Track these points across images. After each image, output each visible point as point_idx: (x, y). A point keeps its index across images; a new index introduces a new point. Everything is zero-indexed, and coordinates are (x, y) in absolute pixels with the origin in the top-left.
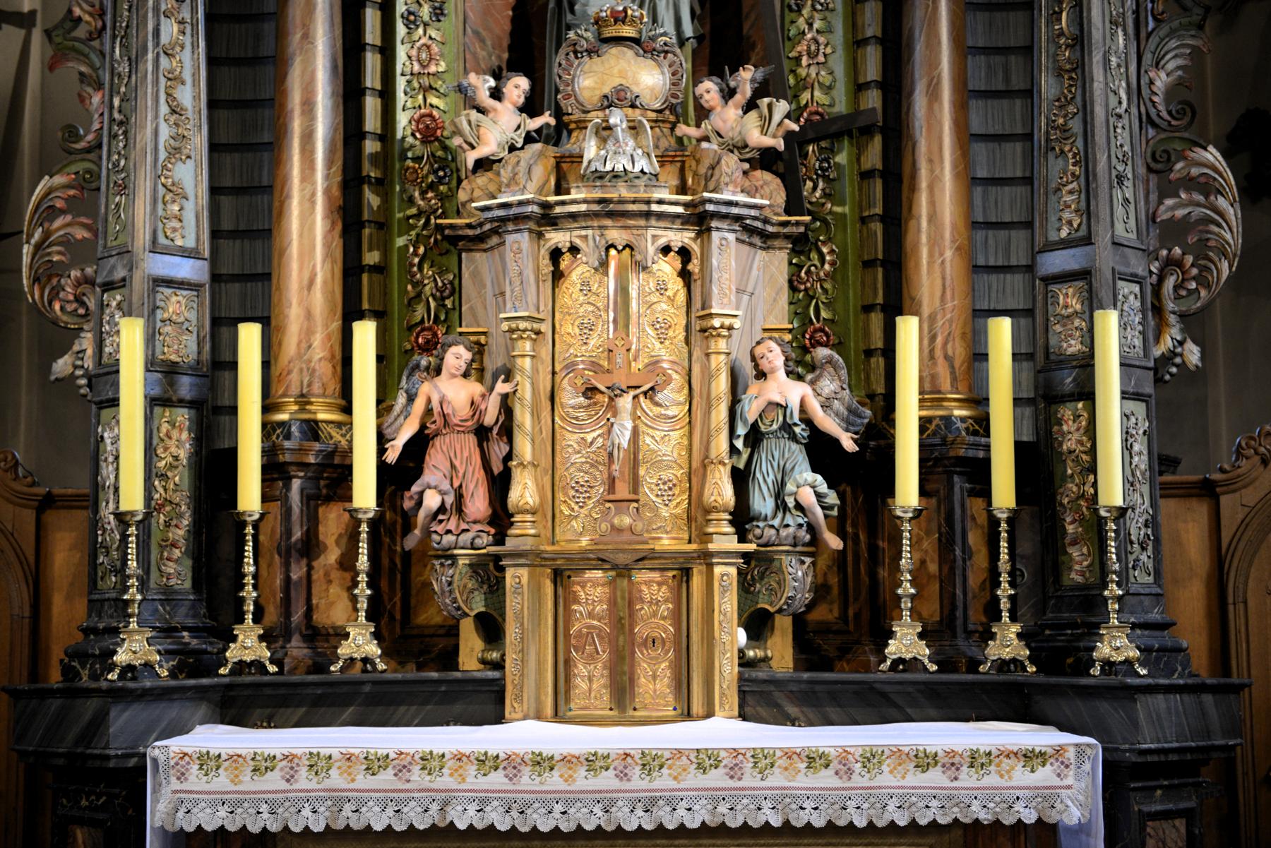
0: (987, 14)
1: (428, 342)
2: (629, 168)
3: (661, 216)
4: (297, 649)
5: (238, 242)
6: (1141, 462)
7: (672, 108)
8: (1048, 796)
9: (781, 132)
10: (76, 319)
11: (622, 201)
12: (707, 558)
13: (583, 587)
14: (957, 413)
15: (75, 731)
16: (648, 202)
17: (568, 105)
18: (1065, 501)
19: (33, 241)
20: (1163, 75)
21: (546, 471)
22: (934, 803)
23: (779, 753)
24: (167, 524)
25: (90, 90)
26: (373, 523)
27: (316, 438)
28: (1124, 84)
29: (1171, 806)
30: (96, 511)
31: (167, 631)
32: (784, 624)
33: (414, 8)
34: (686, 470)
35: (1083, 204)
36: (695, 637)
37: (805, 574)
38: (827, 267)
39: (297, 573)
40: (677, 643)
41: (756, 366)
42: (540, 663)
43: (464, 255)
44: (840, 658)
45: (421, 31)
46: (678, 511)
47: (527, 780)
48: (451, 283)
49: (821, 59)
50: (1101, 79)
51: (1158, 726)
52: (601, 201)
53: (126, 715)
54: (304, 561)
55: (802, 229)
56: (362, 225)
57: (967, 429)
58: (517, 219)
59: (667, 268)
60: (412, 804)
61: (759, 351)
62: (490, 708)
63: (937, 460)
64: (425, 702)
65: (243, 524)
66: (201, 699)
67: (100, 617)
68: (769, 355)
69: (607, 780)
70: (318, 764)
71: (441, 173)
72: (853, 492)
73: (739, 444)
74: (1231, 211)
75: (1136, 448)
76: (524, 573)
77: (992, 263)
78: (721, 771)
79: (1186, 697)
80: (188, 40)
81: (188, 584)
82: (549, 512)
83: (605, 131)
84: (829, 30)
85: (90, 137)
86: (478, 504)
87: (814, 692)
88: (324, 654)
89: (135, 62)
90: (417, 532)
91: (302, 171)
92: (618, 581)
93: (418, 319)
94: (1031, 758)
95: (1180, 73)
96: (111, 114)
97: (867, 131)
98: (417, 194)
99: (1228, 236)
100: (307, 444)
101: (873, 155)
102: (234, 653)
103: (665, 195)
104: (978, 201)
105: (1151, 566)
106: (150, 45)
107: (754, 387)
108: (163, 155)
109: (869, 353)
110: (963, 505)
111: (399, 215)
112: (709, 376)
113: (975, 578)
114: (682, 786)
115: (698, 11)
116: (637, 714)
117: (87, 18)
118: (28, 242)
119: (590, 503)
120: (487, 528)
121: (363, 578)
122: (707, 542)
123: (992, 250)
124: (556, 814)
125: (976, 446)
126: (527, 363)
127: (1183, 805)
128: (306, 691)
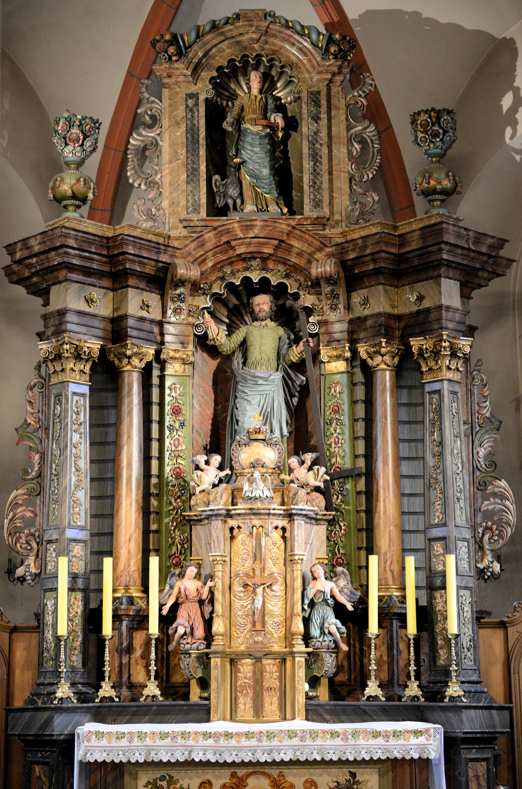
0: (408, 426)
1: (177, 562)
2: (261, 495)
3: (274, 515)
4: (125, 692)
5: (97, 519)
6: (468, 614)
7: (279, 467)
8: (422, 748)
9: (322, 480)
10: (26, 551)
11: (258, 509)
12: (292, 654)
13: (242, 666)
14: (395, 594)
15: (38, 725)
16: (269, 509)
17: (236, 466)
18: (438, 631)
19: (9, 518)
20: (483, 450)
21: (227, 618)
22: (380, 751)
23: (320, 731)
24: (73, 640)
25: (34, 453)
26: (156, 640)
27: (132, 604)
28: (460, 460)
29: (479, 756)
30: (43, 634)
31: (73, 684)
32: (325, 682)
33: (172, 423)
34: (284, 618)
35: (443, 511)
37: (333, 661)
38: (343, 531)
39: (125, 660)
40: (280, 689)
41: (313, 575)
42: (225, 697)
43: (193, 527)
44: (348, 696)
45: (175, 432)
46: (281, 635)
47: (222, 742)
48: (187, 537)
49: (340, 445)
50: (450, 459)
51: (471, 722)
52: (250, 509)
53: (60, 718)
54: (128, 655)
55: (332, 517)
56: (150, 513)
57: (399, 601)
58: (216, 515)
59: (276, 535)
60: (178, 751)
63: (386, 614)
64: (177, 715)
65: (105, 640)
66: (87, 712)
67: (45, 678)
68: (318, 571)
69: (253, 742)
70: (141, 736)
71: (183, 492)
72: (353, 626)
73: (306, 607)
74: (511, 507)
75: (466, 609)
76: (218, 660)
77: (411, 529)
78: (297, 738)
79: (484, 711)
80: (82, 441)
81: (81, 665)
82: (229, 635)
83: (251, 481)
85: (33, 474)
86: (200, 632)
87: (336, 710)
88: (135, 694)
89: (63, 450)
90: (174, 643)
91: (127, 493)
92: (257, 664)
93: (173, 553)
94: (417, 733)
95: (490, 449)
96: (51, 471)
97: (359, 475)
98: (173, 500)
100: (130, 607)
101: (362, 485)
102: (101, 693)
103: (275, 506)
104: (405, 504)
105: (472, 658)
106: (69, 444)
107: (312, 583)
108: (73, 488)
109: (360, 567)
110: (397, 632)
111: (166, 510)
112: (293, 579)
113: (402, 664)
114: (282, 744)
115: (289, 422)
116: (264, 719)
117: (33, 423)
118: (7, 518)
119: (246, 632)
120: (204, 642)
121: (153, 662)
122: (292, 648)
123: (411, 524)
124: (234, 756)
125: (401, 608)
126: (220, 574)
127: (485, 756)
128: (129, 709)
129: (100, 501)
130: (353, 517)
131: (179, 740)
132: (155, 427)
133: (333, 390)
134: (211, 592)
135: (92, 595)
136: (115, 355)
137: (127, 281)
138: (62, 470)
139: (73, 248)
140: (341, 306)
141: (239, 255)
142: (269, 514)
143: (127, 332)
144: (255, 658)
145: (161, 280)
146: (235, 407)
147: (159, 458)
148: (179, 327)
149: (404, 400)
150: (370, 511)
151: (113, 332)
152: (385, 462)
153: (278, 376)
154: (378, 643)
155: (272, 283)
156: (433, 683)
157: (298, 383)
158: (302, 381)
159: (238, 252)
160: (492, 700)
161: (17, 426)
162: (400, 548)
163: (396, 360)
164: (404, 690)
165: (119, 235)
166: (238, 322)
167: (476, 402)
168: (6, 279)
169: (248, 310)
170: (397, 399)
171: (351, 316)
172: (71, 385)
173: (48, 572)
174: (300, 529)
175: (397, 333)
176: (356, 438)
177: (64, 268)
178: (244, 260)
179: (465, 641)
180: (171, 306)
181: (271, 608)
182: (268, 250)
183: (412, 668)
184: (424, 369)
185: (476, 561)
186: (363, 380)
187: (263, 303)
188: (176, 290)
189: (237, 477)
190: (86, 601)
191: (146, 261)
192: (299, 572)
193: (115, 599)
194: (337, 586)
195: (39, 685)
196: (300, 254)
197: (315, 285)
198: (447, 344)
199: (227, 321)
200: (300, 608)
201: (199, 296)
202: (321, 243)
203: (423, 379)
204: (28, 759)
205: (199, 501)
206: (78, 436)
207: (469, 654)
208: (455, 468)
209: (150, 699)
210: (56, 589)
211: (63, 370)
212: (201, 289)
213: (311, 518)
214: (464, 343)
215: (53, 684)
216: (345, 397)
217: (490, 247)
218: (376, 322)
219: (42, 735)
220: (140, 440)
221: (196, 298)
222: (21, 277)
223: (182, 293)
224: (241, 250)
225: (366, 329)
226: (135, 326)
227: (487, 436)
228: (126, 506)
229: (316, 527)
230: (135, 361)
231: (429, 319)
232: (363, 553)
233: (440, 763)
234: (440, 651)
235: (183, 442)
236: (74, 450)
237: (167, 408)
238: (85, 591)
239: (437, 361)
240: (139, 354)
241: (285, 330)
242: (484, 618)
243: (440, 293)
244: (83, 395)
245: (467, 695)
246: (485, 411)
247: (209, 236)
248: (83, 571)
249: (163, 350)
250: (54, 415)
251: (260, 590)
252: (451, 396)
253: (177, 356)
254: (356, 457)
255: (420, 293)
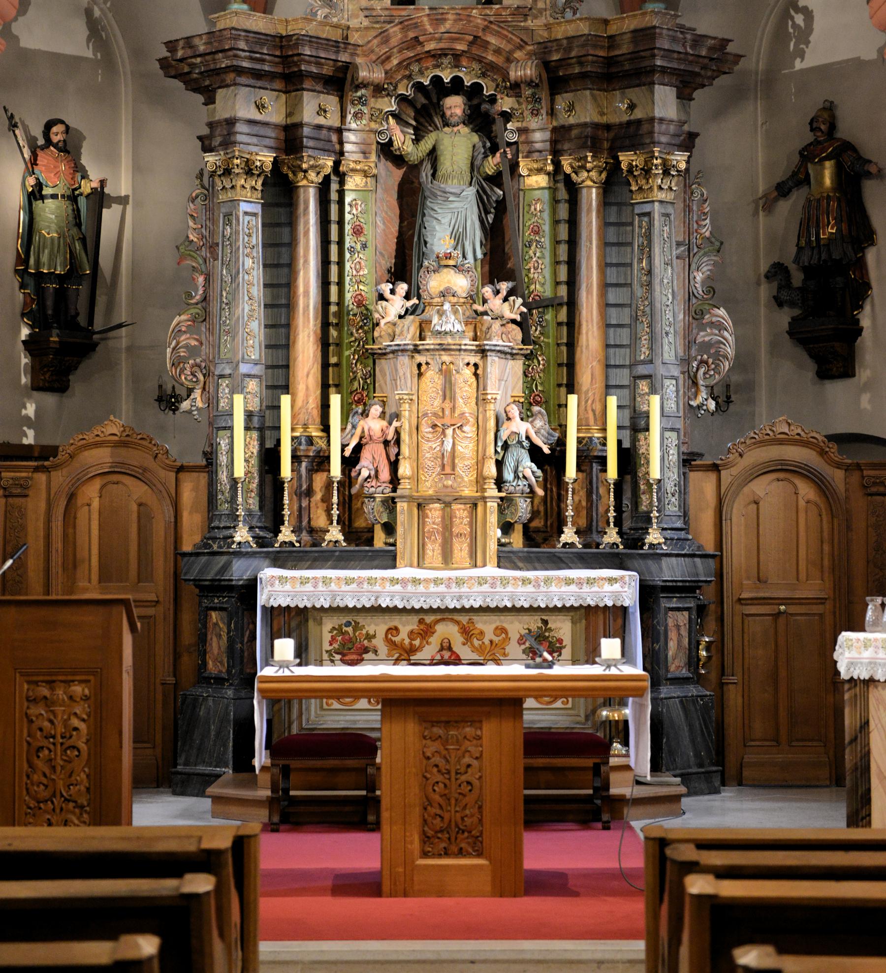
3: (465, 350)
4: (305, 537)
6: (673, 456)
7: (471, 296)
8: (616, 595)
12: (484, 499)
14: (596, 435)
16: (460, 345)
17: (424, 295)
22: (572, 598)
24: (249, 482)
27: (312, 444)
29: (680, 605)
31: (251, 528)
32: (519, 528)
33: (353, 244)
36: (479, 533)
37: (527, 506)
42: (412, 544)
44: (543, 543)
47: (410, 588)
49: (540, 270)
51: (671, 570)
53: (239, 562)
55: (529, 352)
56: (329, 345)
58: (403, 351)
59: (468, 372)
61: (508, 409)
62: (390, 562)
63: (586, 457)
64: (361, 561)
65: (283, 483)
69: (442, 588)
70: (326, 581)
73: (499, 449)
75: (671, 452)
76: (405, 505)
77: (617, 363)
78: (487, 585)
79: (686, 559)
80: (255, 266)
81: (257, 508)
82: (416, 479)
83: (441, 313)
84: (542, 257)
85: (198, 297)
86: (385, 475)
89: (235, 278)
90: (357, 486)
91: (304, 323)
94: (611, 580)
96: (221, 299)
97: (561, 305)
99: (729, 350)
102: (281, 538)
103: (467, 341)
105: (677, 503)
108: (246, 318)
109: (560, 406)
112: (486, 420)
117: (195, 240)
121: (335, 506)
123: (617, 358)
124: (421, 602)
126: (407, 413)
127: (686, 605)
129: (274, 330)
130: (553, 348)
131: (365, 586)
132: (334, 249)
133: (533, 207)
134: (397, 432)
135: (268, 433)
136: (289, 168)
137: (302, 84)
138: (234, 299)
139: (243, 51)
140: (543, 112)
141: (429, 52)
142: (460, 350)
143: (302, 142)
144: (444, 503)
145: (340, 82)
146: (423, 226)
147: (338, 284)
148: (359, 134)
149: (612, 219)
150: (571, 345)
151: (286, 141)
152: (589, 292)
153: (471, 192)
154: (577, 487)
155: (466, 83)
156: (634, 529)
157: (494, 199)
158: (499, 197)
159: (427, 49)
160: (700, 547)
161: (178, 244)
162: (604, 384)
163: (604, 175)
164: (603, 537)
165: (294, 35)
166: (427, 124)
167: (695, 219)
168: (161, 72)
169: (438, 111)
170: (604, 218)
171: (555, 124)
172: (241, 204)
173: (220, 408)
174: (495, 366)
175: (606, 145)
176: (558, 263)
177: (233, 71)
178: (434, 56)
179: (670, 486)
180: (351, 109)
181: (462, 450)
182: (461, 47)
183: (612, 514)
184: (634, 188)
185: (689, 399)
186: (566, 197)
187: (455, 105)
188: (356, 92)
189: (425, 307)
190: (262, 440)
191: (323, 61)
192: (492, 412)
193: (293, 439)
194: (534, 427)
195: (213, 528)
196: (498, 51)
197: (515, 88)
198: (659, 161)
199: (414, 123)
200: (493, 450)
201: (383, 97)
202: (522, 40)
203: (632, 199)
204: (204, 605)
205: (383, 333)
206: (251, 261)
207: (673, 499)
208: (664, 299)
209: (331, 544)
210: (231, 428)
211: (233, 187)
212: (384, 89)
213: (505, 353)
214: (679, 158)
215: (230, 528)
216: (546, 215)
217: (711, 49)
218: (581, 133)
219: (220, 580)
220: (317, 265)
221: (380, 100)
222: (180, 72)
223: (363, 95)
224: (431, 46)
225: (570, 140)
226: (311, 135)
227: (705, 259)
228: (304, 337)
229: (511, 363)
230: (312, 175)
231: (640, 132)
232: (563, 390)
233: (636, 611)
234: (642, 496)
235: (364, 267)
236: (246, 277)
237: (348, 228)
238: (261, 430)
239: (648, 180)
240: (316, 167)
241: (479, 136)
242: (695, 460)
243: (654, 103)
244: (255, 215)
245: (669, 542)
246: (704, 230)
247: (395, 31)
248: (258, 408)
249: (343, 162)
250: (224, 236)
251: (449, 432)
252: (663, 219)
253: (358, 167)
254: (558, 283)
255: (631, 101)
